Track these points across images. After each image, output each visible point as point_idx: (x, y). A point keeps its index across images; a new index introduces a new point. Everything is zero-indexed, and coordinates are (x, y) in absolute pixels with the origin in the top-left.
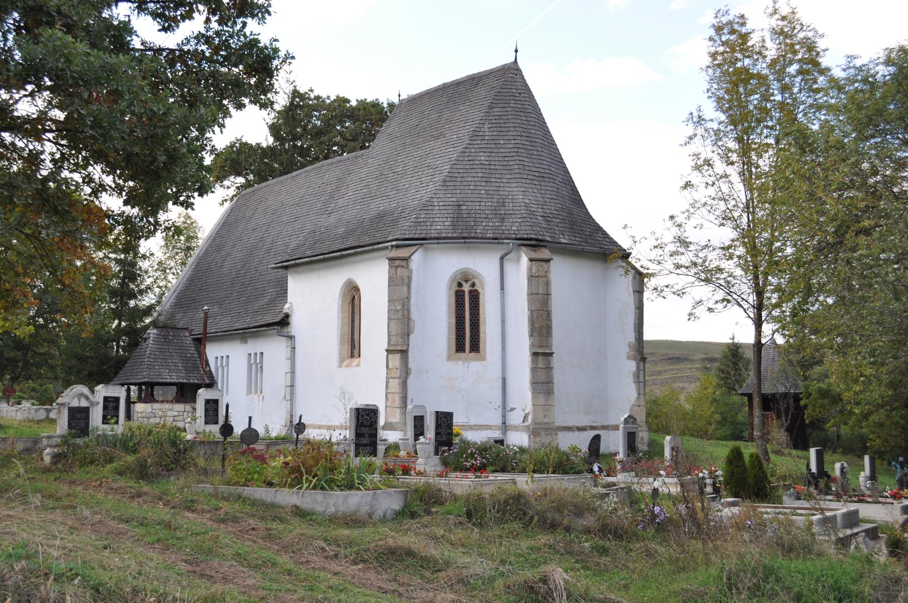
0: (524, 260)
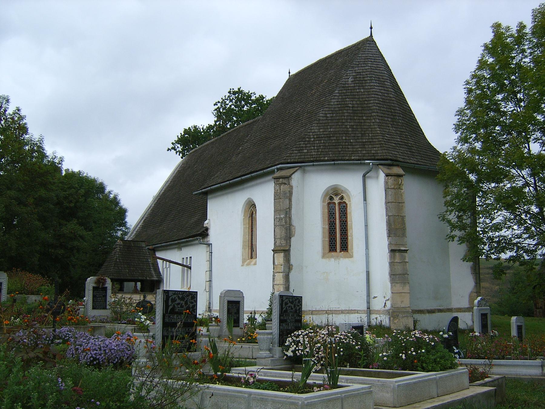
0: (382, 175)
